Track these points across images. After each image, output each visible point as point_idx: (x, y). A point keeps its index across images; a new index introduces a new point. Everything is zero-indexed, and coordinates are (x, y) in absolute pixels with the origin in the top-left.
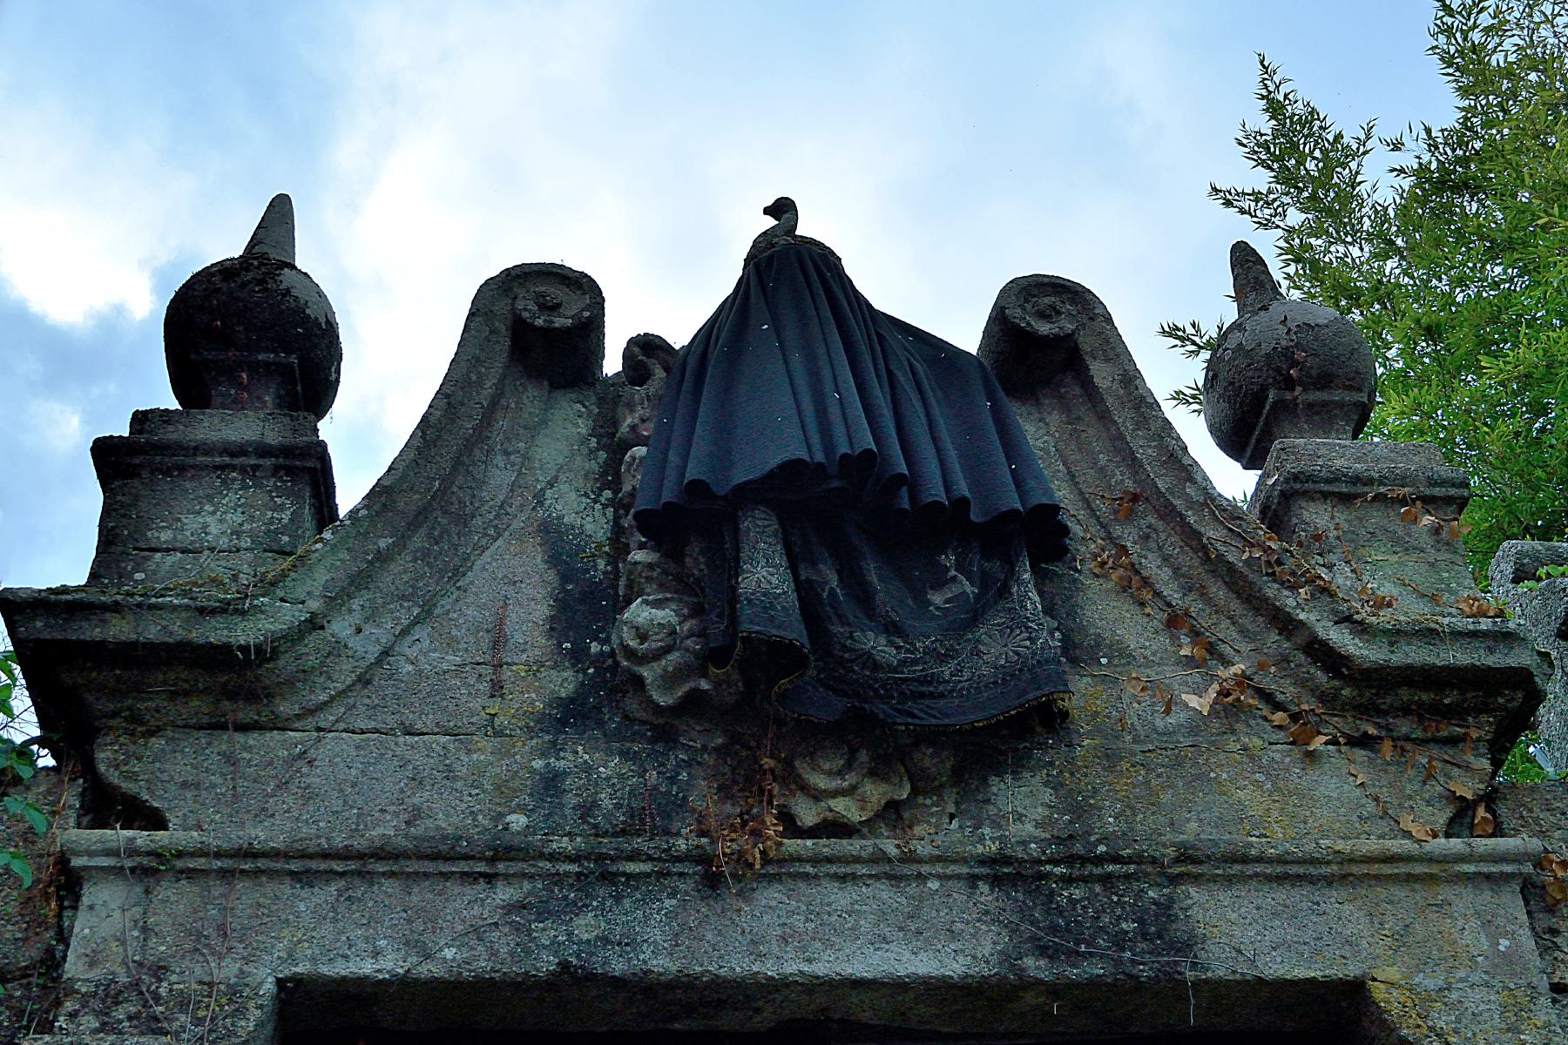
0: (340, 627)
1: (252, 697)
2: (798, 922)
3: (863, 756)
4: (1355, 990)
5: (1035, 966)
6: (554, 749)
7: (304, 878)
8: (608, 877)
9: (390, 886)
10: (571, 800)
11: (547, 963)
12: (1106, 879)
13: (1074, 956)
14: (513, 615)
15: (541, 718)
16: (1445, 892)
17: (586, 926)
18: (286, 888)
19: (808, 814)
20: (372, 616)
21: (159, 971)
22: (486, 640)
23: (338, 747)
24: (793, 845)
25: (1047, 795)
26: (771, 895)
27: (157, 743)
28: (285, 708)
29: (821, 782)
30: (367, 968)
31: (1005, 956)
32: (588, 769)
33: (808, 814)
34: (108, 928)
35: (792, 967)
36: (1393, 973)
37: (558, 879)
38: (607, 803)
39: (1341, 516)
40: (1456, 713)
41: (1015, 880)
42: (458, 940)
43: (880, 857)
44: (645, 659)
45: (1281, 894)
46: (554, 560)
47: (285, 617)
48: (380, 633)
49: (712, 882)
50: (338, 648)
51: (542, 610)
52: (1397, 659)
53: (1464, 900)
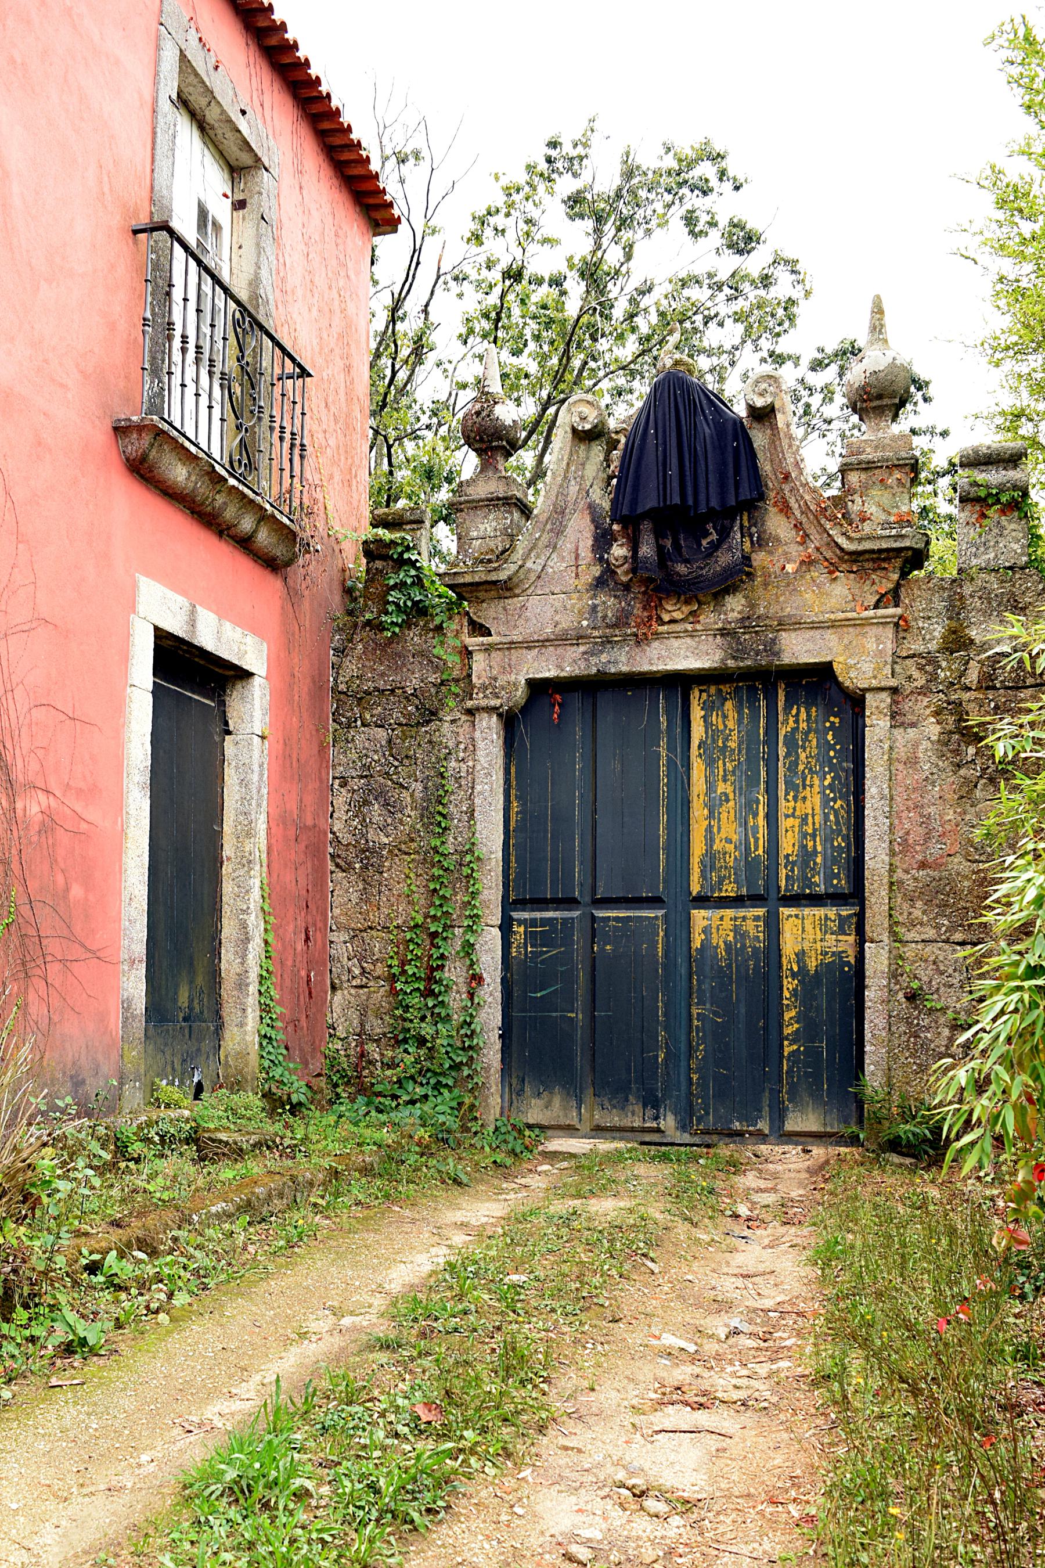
0: (529, 564)
1: (511, 589)
2: (663, 652)
3: (683, 598)
4: (829, 665)
5: (731, 663)
6: (594, 597)
7: (528, 648)
8: (610, 642)
9: (551, 649)
10: (600, 615)
11: (594, 670)
12: (756, 632)
13: (743, 659)
14: (581, 545)
15: (591, 585)
16: (867, 629)
17: (604, 658)
18: (524, 651)
19: (666, 618)
20: (538, 557)
21: (495, 679)
22: (573, 556)
23: (534, 600)
24: (661, 629)
25: (743, 601)
26: (656, 644)
27: (485, 605)
28: (517, 591)
29: (670, 608)
30: (547, 675)
31: (722, 660)
32: (604, 603)
33: (666, 618)
34: (481, 667)
35: (661, 667)
36: (841, 659)
37: (596, 643)
38: (610, 615)
39: (863, 476)
40: (887, 560)
41: (728, 634)
42: (570, 665)
43: (686, 631)
44: (618, 567)
45: (812, 633)
46: (593, 521)
47: (513, 568)
48: (541, 561)
49: (638, 643)
50: (529, 570)
51: (590, 542)
52: (860, 548)
53: (873, 631)
